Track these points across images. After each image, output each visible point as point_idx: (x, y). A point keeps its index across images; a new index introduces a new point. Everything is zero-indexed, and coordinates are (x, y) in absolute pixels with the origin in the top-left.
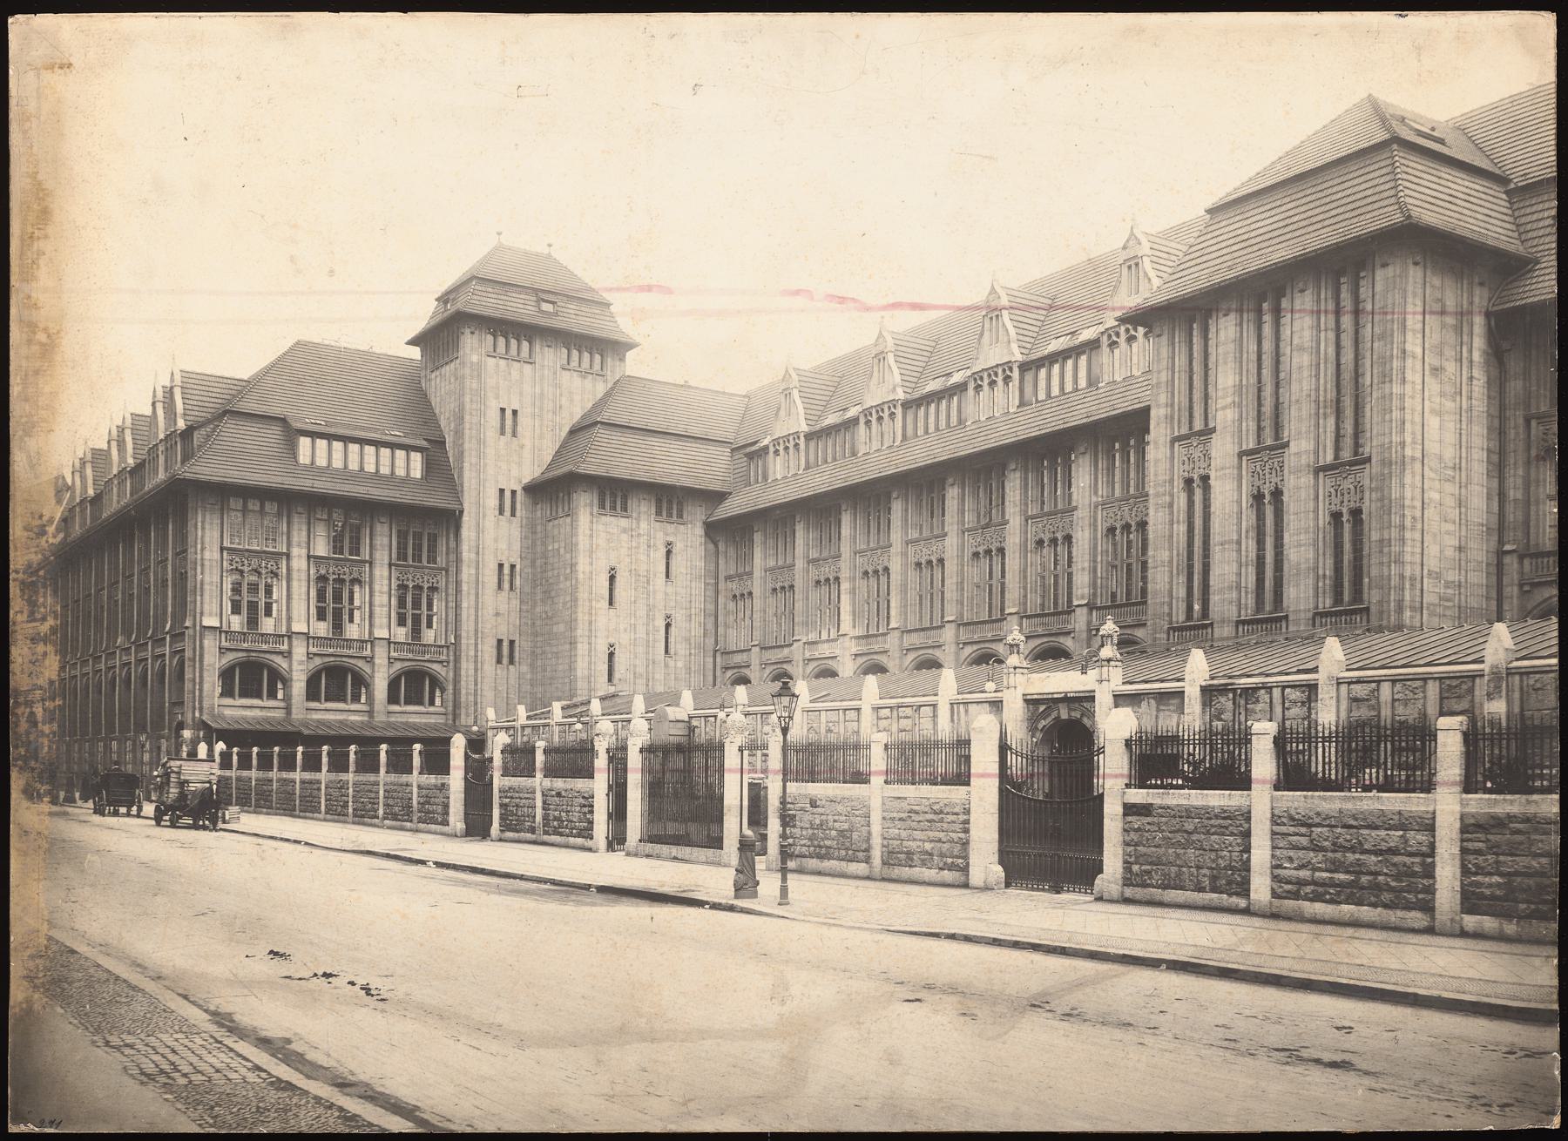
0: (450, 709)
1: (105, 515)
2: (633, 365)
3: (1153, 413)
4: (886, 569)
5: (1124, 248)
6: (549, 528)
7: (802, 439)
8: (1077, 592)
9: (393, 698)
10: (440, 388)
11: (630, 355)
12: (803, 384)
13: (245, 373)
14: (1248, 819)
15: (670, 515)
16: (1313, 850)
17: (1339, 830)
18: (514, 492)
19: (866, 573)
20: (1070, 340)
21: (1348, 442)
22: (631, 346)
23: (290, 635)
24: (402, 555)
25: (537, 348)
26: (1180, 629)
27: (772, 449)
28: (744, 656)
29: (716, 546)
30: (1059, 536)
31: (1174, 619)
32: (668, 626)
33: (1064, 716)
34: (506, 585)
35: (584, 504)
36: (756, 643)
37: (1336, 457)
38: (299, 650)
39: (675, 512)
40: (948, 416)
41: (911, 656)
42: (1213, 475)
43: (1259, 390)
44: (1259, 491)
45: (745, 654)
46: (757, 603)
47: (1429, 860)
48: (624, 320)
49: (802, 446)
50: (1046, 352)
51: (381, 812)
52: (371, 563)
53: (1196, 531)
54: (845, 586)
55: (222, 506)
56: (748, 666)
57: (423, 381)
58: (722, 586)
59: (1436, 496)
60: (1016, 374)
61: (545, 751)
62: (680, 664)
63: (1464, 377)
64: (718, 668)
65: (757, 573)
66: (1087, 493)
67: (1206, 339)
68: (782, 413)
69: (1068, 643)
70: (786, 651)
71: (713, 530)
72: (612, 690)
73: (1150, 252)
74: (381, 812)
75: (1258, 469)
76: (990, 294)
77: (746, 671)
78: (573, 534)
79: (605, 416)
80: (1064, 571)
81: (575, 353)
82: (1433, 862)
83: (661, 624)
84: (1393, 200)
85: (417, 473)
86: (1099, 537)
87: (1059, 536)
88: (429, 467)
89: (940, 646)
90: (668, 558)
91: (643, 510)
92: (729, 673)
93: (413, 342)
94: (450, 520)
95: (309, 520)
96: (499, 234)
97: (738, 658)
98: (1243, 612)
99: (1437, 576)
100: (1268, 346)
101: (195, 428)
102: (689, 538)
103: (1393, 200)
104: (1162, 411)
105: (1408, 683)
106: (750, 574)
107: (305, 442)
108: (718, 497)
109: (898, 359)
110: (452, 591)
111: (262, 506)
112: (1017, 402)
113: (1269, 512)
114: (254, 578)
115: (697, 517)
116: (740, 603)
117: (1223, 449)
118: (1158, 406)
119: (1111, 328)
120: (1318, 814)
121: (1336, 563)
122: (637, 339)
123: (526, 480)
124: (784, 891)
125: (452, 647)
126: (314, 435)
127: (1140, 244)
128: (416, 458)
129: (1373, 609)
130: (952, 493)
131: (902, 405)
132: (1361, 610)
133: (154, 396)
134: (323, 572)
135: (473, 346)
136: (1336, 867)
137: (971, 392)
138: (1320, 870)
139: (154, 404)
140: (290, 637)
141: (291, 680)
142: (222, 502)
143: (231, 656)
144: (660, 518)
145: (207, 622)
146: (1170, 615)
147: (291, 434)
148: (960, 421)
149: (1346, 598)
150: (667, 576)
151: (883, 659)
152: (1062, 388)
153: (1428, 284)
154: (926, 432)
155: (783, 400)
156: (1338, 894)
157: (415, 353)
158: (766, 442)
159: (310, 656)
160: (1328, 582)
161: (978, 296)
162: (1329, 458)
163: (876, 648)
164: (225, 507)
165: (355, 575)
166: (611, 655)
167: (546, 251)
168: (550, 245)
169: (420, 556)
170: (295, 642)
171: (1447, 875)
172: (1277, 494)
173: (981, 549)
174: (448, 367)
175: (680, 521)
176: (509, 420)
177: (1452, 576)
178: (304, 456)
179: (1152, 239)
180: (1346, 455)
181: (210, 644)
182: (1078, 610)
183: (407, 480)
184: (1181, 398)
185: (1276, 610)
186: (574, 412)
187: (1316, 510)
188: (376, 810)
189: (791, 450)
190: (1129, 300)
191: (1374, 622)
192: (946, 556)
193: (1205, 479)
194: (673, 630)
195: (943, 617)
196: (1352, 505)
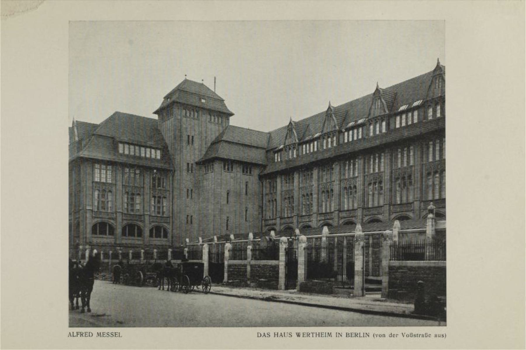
2: (233, 121)
4: (276, 200)
7: (297, 145)
9: (151, 236)
11: (231, 118)
18: (192, 164)
20: (409, 106)
22: (232, 114)
23: (116, 213)
28: (274, 221)
29: (262, 183)
32: (246, 211)
35: (217, 166)
38: (119, 219)
39: (249, 172)
41: (284, 226)
48: (230, 106)
54: (315, 196)
61: (251, 250)
65: (279, 192)
69: (411, 214)
70: (291, 219)
71: (261, 177)
77: (275, 227)
79: (224, 138)
81: (213, 117)
83: (244, 210)
85: (159, 157)
87: (352, 186)
88: (163, 156)
89: (332, 219)
96: (186, 75)
97: (270, 222)
102: (253, 179)
106: (276, 193)
107: (121, 146)
108: (264, 167)
110: (171, 198)
111: (106, 167)
115: (256, 172)
122: (233, 112)
123: (197, 160)
126: (124, 143)
128: (159, 152)
131: (338, 132)
134: (127, 191)
135: (178, 112)
140: (116, 214)
141: (116, 229)
143: (96, 220)
145: (88, 208)
151: (331, 221)
157: (156, 117)
159: (123, 220)
163: (328, 217)
166: (227, 221)
167: (201, 82)
168: (203, 80)
170: (118, 214)
173: (287, 196)
181: (88, 215)
183: (155, 160)
186: (212, 137)
192: (313, 192)
194: (248, 212)
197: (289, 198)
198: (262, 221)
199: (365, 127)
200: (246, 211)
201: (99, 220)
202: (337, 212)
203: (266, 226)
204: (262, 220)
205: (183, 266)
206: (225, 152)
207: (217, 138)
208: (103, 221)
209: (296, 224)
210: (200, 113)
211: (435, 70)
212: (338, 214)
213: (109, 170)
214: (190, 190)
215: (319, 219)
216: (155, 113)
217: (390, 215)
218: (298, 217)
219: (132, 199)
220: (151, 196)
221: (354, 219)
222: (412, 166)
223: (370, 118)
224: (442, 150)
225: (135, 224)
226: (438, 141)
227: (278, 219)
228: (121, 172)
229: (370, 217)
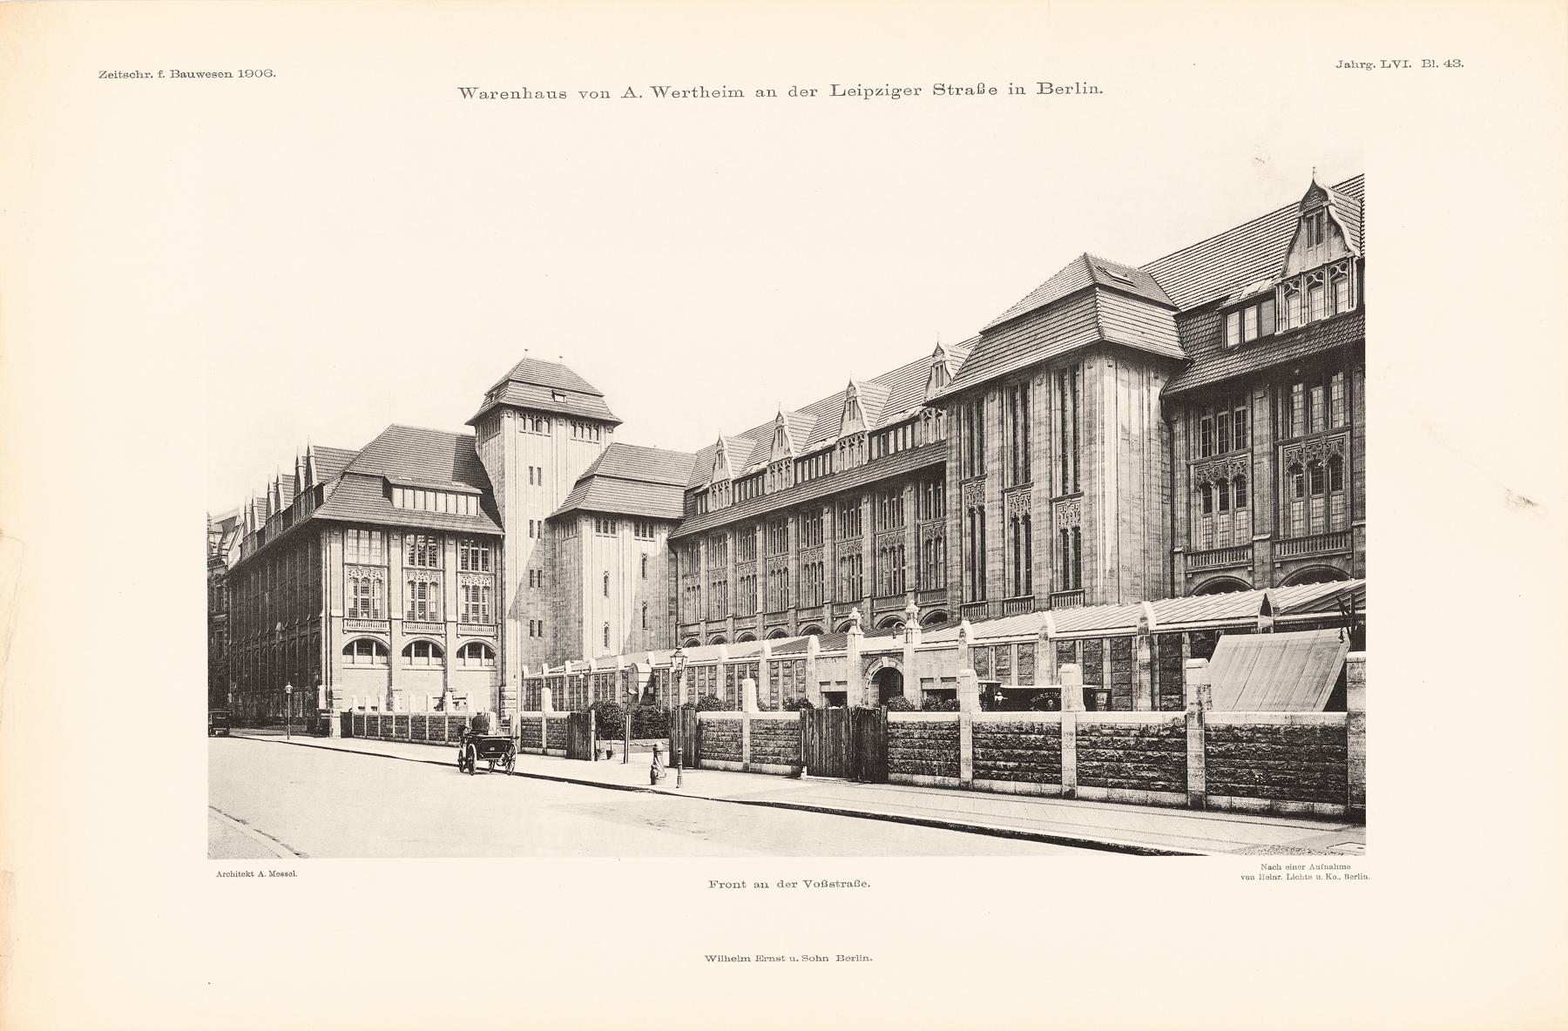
0: (499, 667)
1: (295, 523)
3: (948, 465)
5: (934, 356)
6: (564, 546)
8: (907, 583)
10: (489, 454)
12: (865, 394)
13: (357, 446)
14: (959, 730)
15: (644, 536)
16: (996, 748)
17: (1009, 736)
18: (539, 522)
19: (773, 572)
21: (1070, 484)
24: (465, 566)
25: (554, 427)
26: (970, 606)
27: (711, 490)
30: (896, 545)
31: (964, 600)
32: (644, 609)
33: (886, 665)
34: (536, 584)
35: (587, 528)
36: (828, 601)
37: (1064, 493)
40: (817, 471)
42: (986, 505)
43: (1015, 449)
44: (1015, 515)
45: (722, 623)
46: (704, 594)
47: (1059, 753)
48: (614, 407)
49: (731, 488)
50: (886, 425)
51: (446, 736)
52: (444, 572)
53: (977, 542)
54: (760, 580)
55: (343, 536)
56: (822, 620)
57: (477, 449)
58: (680, 582)
59: (1126, 517)
60: (866, 439)
62: (653, 634)
63: (1145, 439)
64: (679, 636)
65: (703, 573)
66: (913, 518)
67: (1073, 384)
68: (717, 466)
72: (606, 652)
73: (950, 358)
74: (446, 736)
75: (1026, 499)
76: (849, 386)
78: (579, 547)
79: (600, 471)
80: (820, 582)
81: (579, 429)
82: (1061, 754)
84: (1094, 325)
86: (921, 546)
87: (896, 545)
90: (643, 564)
91: (626, 532)
92: (686, 640)
93: (469, 423)
94: (496, 541)
95: (402, 544)
97: (692, 629)
98: (1007, 595)
99: (1129, 570)
100: (1020, 420)
101: (324, 485)
103: (1094, 325)
104: (954, 464)
105: (1092, 641)
106: (698, 573)
107: (397, 493)
109: (864, 401)
112: (868, 458)
113: (1022, 528)
114: (365, 584)
115: (662, 536)
116: (692, 593)
117: (992, 489)
118: (951, 461)
119: (1337, 261)
120: (998, 726)
121: (1065, 562)
123: (548, 515)
124: (679, 778)
125: (500, 626)
126: (403, 487)
127: (943, 353)
129: (1087, 591)
130: (866, 508)
132: (1080, 593)
133: (297, 463)
136: (1008, 758)
137: (711, 493)
138: (1000, 760)
139: (297, 469)
140: (390, 622)
142: (343, 533)
144: (637, 538)
146: (962, 597)
147: (388, 489)
148: (706, 511)
149: (1071, 586)
150: (643, 576)
152: (701, 510)
153: (1118, 380)
154: (758, 495)
155: (717, 458)
156: (1010, 775)
157: (471, 431)
158: (707, 486)
160: (1059, 574)
161: (767, 417)
162: (1060, 494)
164: (345, 536)
165: (434, 580)
169: (477, 566)
171: (1069, 759)
172: (1027, 518)
173: (846, 555)
174: (493, 439)
175: (651, 539)
176: (535, 475)
177: (1139, 569)
178: (397, 502)
179: (861, 385)
180: (1070, 491)
182: (909, 594)
184: (965, 455)
185: (1027, 594)
187: (1051, 528)
188: (443, 735)
189: (723, 491)
190: (934, 392)
191: (1088, 598)
192: (824, 560)
193: (981, 508)
195: (861, 595)
196: (1074, 525)
197: (720, 583)
198: (676, 628)
199: (1267, 307)
200: (644, 609)
201: (357, 636)
202: (793, 611)
203: (683, 637)
204: (677, 625)
205: (1209, 745)
206: (601, 497)
207: (591, 470)
208: (366, 637)
209: (830, 622)
210: (553, 421)
211: (1307, 197)
212: (796, 614)
213: (376, 539)
214: (536, 571)
215: (766, 623)
216: (469, 423)
217: (873, 617)
218: (707, 623)
219: (422, 595)
220: (460, 586)
221: (819, 624)
222: (1318, 436)
223: (841, 436)
224: (1354, 402)
225: (429, 640)
226: (1341, 376)
227: (703, 624)
228: (399, 543)
229: (932, 609)
